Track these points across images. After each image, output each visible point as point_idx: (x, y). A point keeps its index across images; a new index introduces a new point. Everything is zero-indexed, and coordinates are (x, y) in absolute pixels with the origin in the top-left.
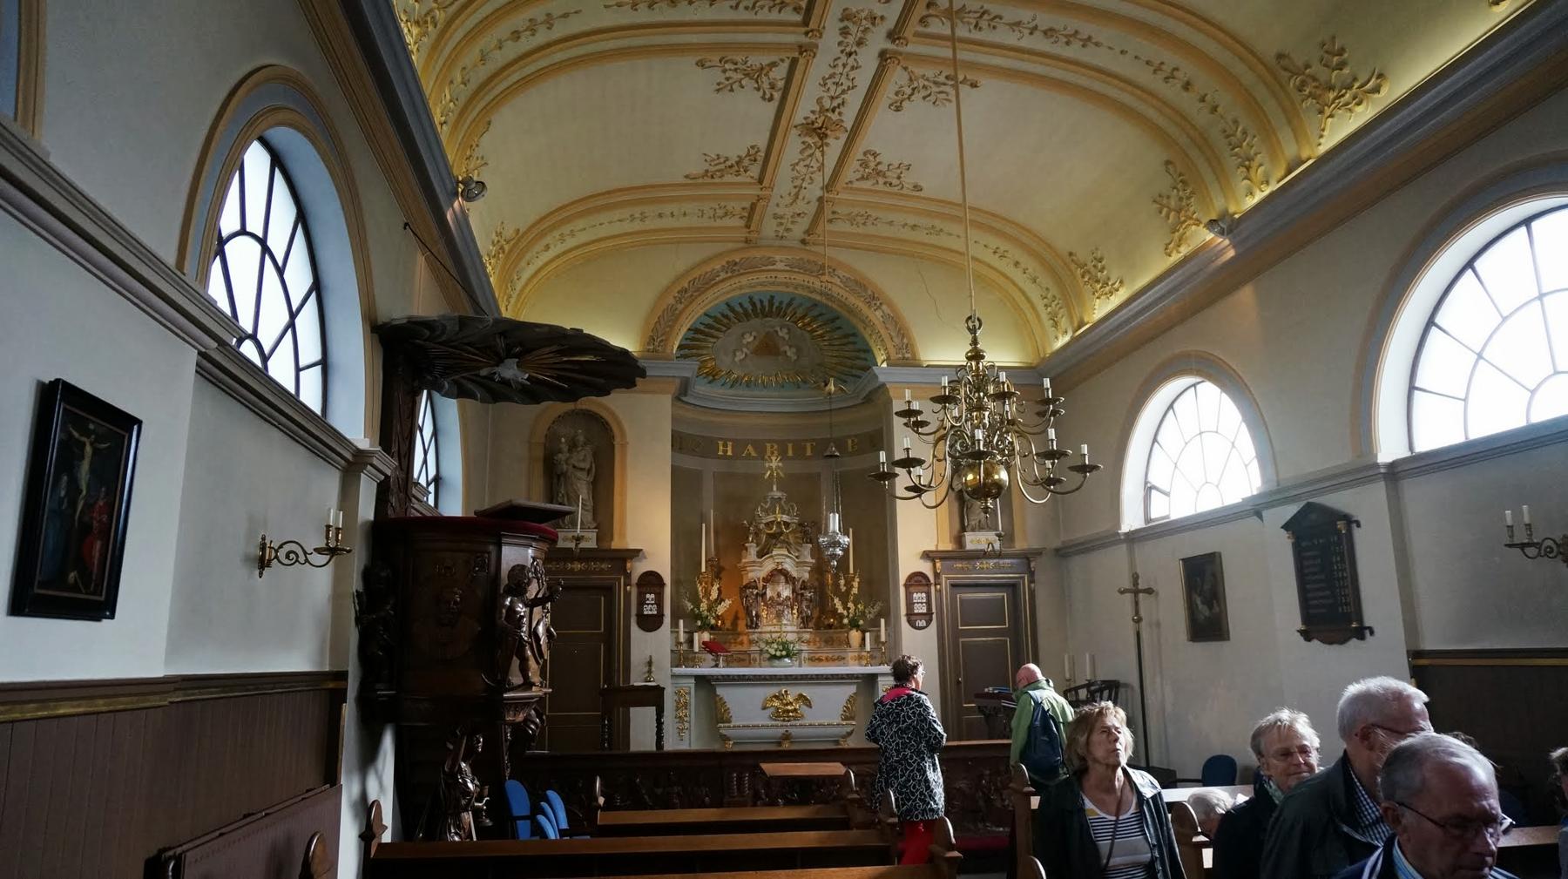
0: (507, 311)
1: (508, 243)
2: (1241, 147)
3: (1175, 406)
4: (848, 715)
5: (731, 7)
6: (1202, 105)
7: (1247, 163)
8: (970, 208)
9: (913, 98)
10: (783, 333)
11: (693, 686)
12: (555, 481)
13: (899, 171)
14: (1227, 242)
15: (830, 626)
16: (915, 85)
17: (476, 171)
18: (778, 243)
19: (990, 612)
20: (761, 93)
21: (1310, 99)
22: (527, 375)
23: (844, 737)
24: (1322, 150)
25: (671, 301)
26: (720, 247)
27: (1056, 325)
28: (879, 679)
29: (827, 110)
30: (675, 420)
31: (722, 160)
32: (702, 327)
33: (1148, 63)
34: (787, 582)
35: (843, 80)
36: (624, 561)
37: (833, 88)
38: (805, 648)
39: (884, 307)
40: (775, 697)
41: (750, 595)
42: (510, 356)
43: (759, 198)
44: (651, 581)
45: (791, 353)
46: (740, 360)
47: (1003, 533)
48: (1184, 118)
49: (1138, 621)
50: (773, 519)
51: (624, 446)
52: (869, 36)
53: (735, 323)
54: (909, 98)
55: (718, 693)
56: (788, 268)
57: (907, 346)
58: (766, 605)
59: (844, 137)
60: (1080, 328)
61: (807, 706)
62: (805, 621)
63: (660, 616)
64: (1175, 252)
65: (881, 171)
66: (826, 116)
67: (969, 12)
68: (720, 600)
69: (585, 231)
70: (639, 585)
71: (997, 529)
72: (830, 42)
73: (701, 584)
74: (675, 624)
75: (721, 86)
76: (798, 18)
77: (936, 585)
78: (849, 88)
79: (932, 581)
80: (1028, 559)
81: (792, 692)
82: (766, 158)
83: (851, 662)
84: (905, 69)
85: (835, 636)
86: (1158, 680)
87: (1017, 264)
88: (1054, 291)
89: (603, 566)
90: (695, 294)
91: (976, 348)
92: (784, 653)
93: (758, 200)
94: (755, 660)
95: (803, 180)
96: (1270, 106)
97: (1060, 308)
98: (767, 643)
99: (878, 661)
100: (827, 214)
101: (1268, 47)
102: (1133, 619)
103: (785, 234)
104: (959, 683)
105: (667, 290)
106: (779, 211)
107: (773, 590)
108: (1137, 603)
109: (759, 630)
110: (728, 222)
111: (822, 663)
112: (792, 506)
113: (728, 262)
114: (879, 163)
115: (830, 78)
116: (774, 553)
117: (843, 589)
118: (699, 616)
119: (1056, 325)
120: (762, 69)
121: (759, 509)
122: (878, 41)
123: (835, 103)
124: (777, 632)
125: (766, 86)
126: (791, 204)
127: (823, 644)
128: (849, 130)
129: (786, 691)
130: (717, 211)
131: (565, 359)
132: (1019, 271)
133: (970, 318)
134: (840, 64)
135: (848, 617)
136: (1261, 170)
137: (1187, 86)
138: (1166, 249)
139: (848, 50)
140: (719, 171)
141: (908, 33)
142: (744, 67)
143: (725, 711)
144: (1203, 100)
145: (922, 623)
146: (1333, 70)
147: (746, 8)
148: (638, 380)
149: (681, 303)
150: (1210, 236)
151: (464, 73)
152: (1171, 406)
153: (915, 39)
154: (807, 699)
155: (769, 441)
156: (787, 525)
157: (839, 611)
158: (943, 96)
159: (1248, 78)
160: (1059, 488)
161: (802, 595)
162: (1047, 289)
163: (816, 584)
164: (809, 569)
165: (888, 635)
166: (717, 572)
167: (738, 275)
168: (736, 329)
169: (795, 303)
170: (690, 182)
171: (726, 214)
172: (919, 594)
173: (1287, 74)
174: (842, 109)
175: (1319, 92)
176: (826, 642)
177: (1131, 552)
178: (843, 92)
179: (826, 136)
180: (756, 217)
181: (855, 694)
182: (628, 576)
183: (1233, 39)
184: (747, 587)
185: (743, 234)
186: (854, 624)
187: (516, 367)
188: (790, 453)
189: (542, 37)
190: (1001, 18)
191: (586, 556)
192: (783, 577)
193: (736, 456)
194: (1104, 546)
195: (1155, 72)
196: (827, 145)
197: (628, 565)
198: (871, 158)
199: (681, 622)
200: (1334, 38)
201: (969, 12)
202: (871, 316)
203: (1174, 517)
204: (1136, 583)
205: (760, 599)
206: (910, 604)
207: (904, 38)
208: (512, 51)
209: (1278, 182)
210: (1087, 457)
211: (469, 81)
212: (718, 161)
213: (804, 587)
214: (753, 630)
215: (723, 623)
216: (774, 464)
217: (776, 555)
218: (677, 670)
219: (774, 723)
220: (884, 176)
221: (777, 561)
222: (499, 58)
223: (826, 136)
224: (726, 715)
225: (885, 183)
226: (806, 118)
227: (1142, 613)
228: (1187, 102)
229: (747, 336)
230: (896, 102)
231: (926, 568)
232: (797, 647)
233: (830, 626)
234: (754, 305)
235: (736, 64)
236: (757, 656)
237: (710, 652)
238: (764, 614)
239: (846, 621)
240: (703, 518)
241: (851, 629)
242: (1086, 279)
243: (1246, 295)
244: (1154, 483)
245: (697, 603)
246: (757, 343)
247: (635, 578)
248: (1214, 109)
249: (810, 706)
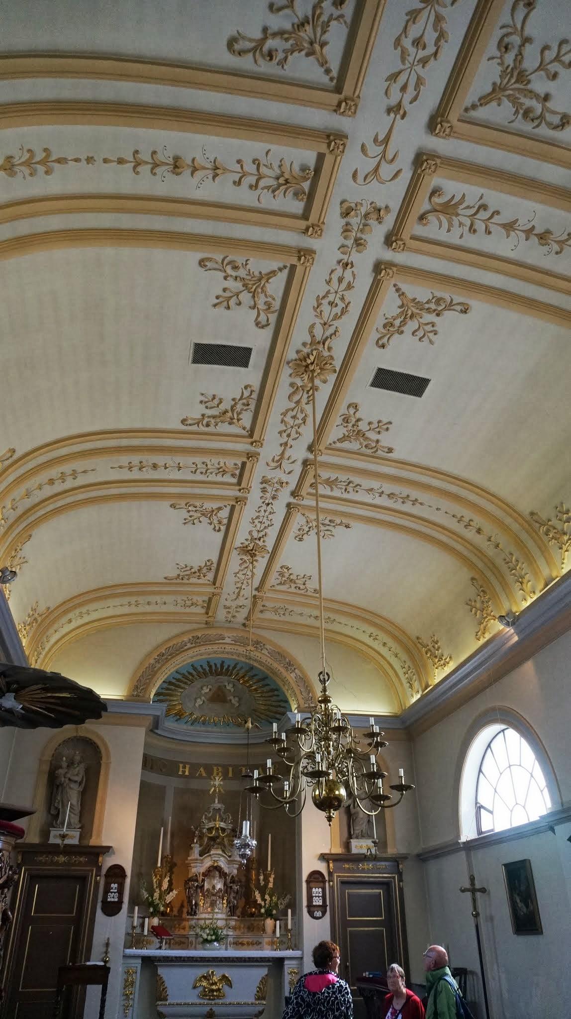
0: (35, 663)
1: (41, 616)
2: (516, 569)
3: (492, 745)
4: (261, 995)
5: (192, 472)
6: (489, 543)
7: (520, 580)
8: (324, 599)
9: (309, 533)
10: (229, 687)
11: (139, 966)
12: (55, 789)
13: (304, 579)
14: (512, 631)
15: (252, 915)
16: (311, 525)
17: (19, 566)
18: (227, 625)
19: (369, 906)
20: (212, 526)
21: (553, 540)
22: (21, 706)
24: (564, 571)
25: (152, 661)
26: (188, 627)
27: (411, 686)
28: (286, 962)
29: (256, 539)
30: (147, 745)
31: (188, 568)
32: (174, 681)
33: (453, 516)
34: (220, 877)
35: (265, 520)
36: (97, 855)
37: (259, 525)
38: (231, 934)
39: (296, 670)
40: (204, 977)
41: (192, 886)
42: (9, 691)
43: (214, 594)
44: (117, 872)
45: (235, 701)
47: (377, 841)
48: (480, 552)
49: (476, 916)
51: (108, 765)
52: (279, 494)
53: (196, 679)
54: (307, 533)
56: (233, 642)
57: (312, 698)
58: (203, 895)
59: (267, 556)
60: (426, 688)
61: (228, 985)
62: (232, 910)
63: (120, 902)
64: (482, 637)
65: (292, 580)
66: (255, 543)
67: (340, 482)
68: (170, 889)
69: (98, 611)
70: (106, 876)
71: (374, 838)
72: (255, 496)
73: (156, 877)
74: (131, 911)
75: (187, 521)
76: (235, 481)
77: (329, 881)
78: (269, 526)
79: (327, 878)
80: (397, 862)
81: (218, 973)
82: (217, 568)
84: (304, 515)
86: (495, 967)
87: (384, 644)
88: (408, 663)
89: (81, 859)
90: (169, 657)
91: (325, 694)
92: (214, 937)
93: (213, 596)
94: (191, 943)
95: (242, 583)
96: (530, 544)
97: (414, 675)
98: (202, 928)
99: (286, 946)
100: (259, 607)
101: (525, 506)
102: (472, 914)
103: (232, 619)
104: (347, 967)
105: (149, 655)
106: (228, 604)
107: (209, 883)
108: (474, 900)
109: (197, 917)
110: (193, 610)
111: (245, 947)
112: (229, 816)
113: (193, 637)
114: (291, 574)
115: (256, 519)
116: (212, 852)
117: (262, 883)
118: (151, 904)
119: (411, 686)
120: (213, 511)
121: (204, 817)
122: (285, 497)
123: (261, 535)
125: (216, 522)
126: (236, 599)
127: (246, 930)
128: (270, 552)
129: (213, 972)
130: (187, 602)
131: (49, 695)
132: (386, 649)
133: (321, 673)
134: (263, 511)
136: (530, 583)
137: (479, 531)
138: (477, 635)
139: (267, 502)
140: (187, 575)
141: (303, 492)
142: (201, 509)
143: (164, 989)
144: (489, 540)
145: (318, 914)
146: (565, 522)
147: (202, 473)
148: (103, 713)
149: (159, 663)
150: (501, 627)
151: (14, 503)
152: (489, 746)
153: (308, 496)
155: (243, 766)
156: (223, 830)
158: (329, 533)
159: (515, 527)
160: (387, 803)
161: (231, 887)
162: (405, 662)
163: (243, 879)
165: (294, 924)
166: (171, 866)
167: (199, 646)
168: (198, 684)
169: (238, 667)
170: (168, 581)
171: (192, 604)
172: (317, 889)
173: (537, 525)
174: (265, 538)
175: (558, 536)
177: (468, 857)
178: (265, 528)
179: (255, 555)
180: (213, 605)
181: (266, 975)
182: (99, 868)
183: (509, 508)
184: (191, 880)
185: (204, 618)
186: (269, 914)
187: (13, 699)
188: (230, 775)
189: (69, 484)
190: (360, 486)
191: (69, 850)
192: (217, 873)
193: (192, 776)
194: (449, 853)
195: (459, 522)
196: (256, 561)
197: (100, 859)
198: (286, 570)
199: (137, 908)
200: (562, 503)
201: (340, 482)
202: (288, 678)
203: (497, 830)
204: (473, 884)
205: (199, 890)
206: (310, 897)
207: (301, 496)
208: (48, 491)
209: (540, 592)
210: (403, 778)
211: (17, 507)
212: (185, 569)
214: (192, 917)
215: (171, 910)
216: (217, 783)
217: (213, 854)
218: (129, 951)
219: (202, 1001)
220: (295, 583)
221: (214, 859)
222: (38, 496)
223: (255, 555)
225: (296, 587)
226: (242, 544)
227: (480, 910)
228: (479, 540)
229: (205, 688)
230: (299, 535)
231: (322, 867)
232: (225, 932)
233: (252, 915)
234: (210, 667)
235: (196, 507)
236: (194, 939)
237: (156, 936)
238: (201, 903)
239: (263, 910)
240: (164, 824)
241: (267, 918)
242: (428, 655)
243: (529, 667)
244: (482, 804)
245: (151, 892)
246: (211, 693)
247: (104, 871)
248: (497, 546)
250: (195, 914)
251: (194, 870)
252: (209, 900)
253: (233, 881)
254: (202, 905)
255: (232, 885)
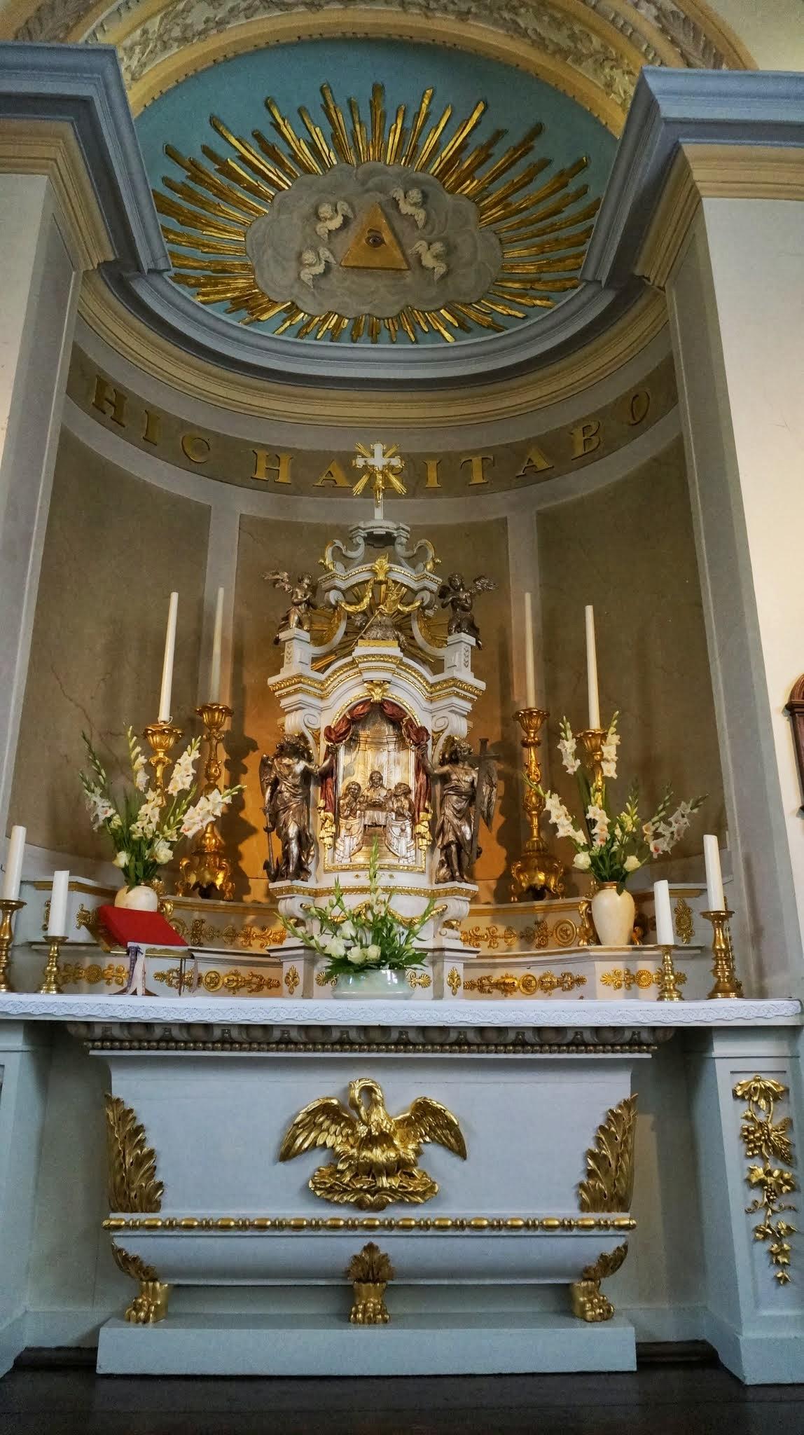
15: (538, 893)
23: (586, 1274)
28: (720, 1048)
46: (316, 278)
50: (366, 576)
55: (116, 1093)
68: (190, 798)
83: (600, 987)
85: (551, 921)
109: (311, 884)
116: (359, 651)
117: (572, 765)
124: (363, 890)
127: (516, 943)
135: (588, 847)
143: (139, 1162)
154: (450, 1125)
157: (561, 833)
161: (445, 778)
164: (468, 706)
176: (527, 937)
181: (627, 1105)
188: (433, 480)
205: (315, 791)
213: (453, 756)
221: (368, 676)
224: (139, 1182)
233: (538, 893)
236: (300, 966)
238: (324, 834)
249: (460, 1151)
250: (302, 871)
251: (292, 723)
252: (356, 824)
253: (453, 756)
254: (328, 841)
255: (446, 768)
